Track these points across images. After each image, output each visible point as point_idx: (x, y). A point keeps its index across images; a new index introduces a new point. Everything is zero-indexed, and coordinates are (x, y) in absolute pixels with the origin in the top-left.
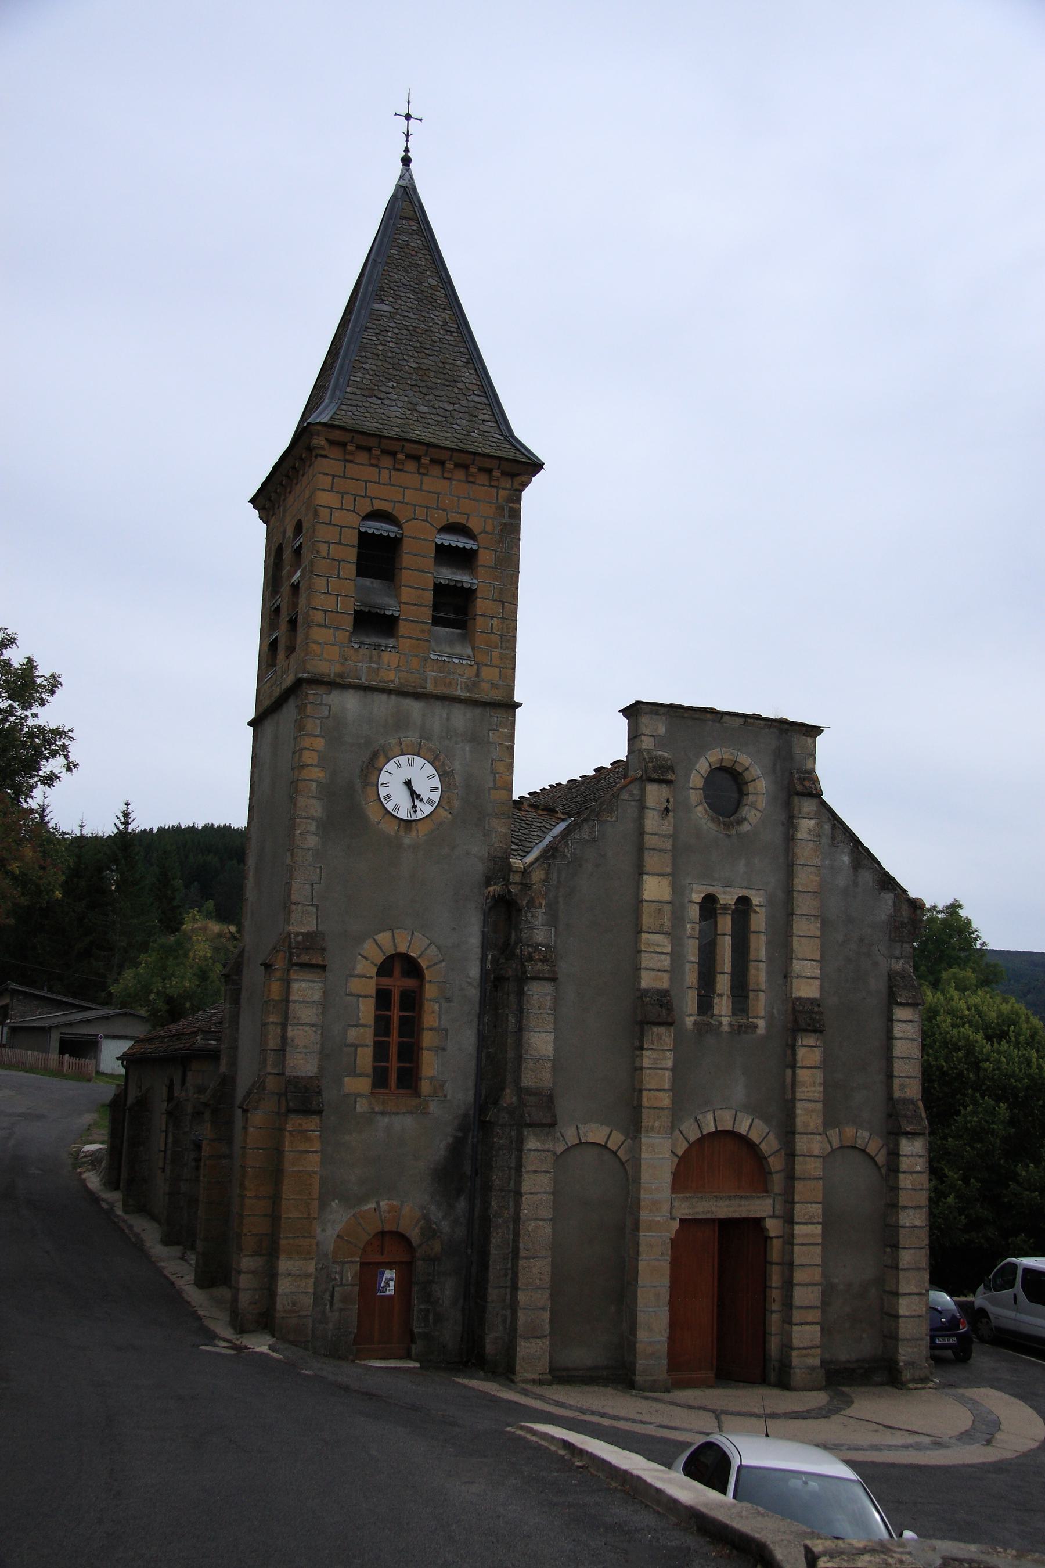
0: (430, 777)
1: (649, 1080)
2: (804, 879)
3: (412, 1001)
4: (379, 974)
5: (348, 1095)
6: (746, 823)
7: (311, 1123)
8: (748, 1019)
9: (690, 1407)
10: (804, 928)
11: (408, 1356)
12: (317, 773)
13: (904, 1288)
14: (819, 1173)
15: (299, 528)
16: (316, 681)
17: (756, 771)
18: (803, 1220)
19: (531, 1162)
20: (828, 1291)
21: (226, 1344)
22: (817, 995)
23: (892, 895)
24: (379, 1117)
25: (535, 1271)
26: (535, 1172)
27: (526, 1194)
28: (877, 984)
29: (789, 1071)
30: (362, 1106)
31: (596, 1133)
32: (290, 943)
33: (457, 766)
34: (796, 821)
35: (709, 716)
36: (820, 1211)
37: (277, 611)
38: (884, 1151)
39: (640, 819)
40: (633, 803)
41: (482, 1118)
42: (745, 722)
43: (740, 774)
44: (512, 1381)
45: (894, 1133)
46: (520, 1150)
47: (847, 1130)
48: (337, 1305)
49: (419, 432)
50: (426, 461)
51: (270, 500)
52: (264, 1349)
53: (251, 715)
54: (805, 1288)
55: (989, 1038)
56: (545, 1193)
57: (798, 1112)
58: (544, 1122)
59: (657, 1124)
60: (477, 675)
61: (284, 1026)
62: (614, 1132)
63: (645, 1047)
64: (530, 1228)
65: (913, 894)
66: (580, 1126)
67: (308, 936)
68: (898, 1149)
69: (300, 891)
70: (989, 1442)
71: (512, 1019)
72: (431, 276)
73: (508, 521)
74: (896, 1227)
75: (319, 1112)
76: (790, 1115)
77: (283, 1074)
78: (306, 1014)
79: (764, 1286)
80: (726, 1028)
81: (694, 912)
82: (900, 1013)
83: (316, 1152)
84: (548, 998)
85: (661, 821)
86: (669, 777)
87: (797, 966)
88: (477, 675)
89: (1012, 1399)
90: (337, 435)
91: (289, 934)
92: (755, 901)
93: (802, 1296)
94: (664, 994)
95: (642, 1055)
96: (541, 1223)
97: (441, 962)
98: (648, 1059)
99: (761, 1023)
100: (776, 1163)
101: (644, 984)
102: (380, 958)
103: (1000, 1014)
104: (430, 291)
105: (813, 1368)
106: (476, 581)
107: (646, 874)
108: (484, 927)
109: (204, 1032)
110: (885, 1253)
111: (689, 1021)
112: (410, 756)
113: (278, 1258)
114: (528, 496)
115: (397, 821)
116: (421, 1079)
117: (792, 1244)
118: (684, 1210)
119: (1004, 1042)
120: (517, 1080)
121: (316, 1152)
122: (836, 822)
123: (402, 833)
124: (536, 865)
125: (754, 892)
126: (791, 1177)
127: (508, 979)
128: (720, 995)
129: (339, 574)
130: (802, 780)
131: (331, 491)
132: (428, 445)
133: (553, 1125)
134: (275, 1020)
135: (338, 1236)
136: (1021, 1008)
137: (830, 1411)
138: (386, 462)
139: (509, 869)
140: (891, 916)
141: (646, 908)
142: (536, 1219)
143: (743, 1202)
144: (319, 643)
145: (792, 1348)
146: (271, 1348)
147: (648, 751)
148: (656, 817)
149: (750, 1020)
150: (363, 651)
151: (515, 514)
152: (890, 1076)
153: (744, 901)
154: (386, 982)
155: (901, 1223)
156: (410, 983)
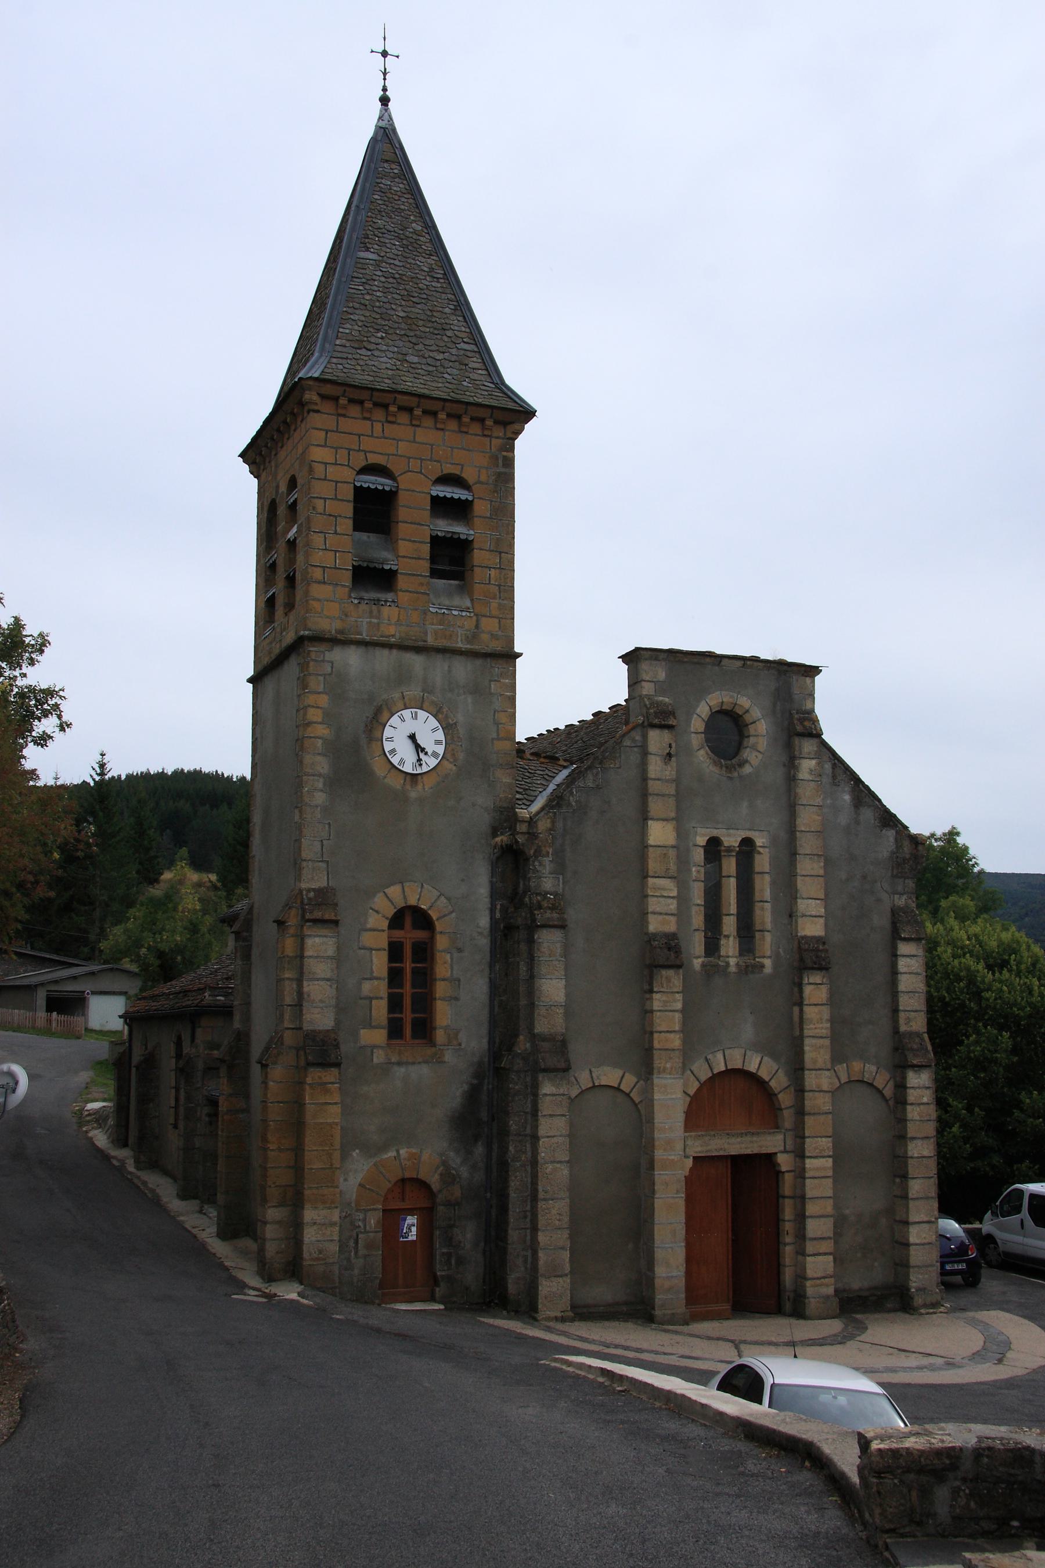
0: (434, 730)
1: (660, 1022)
2: (807, 819)
3: (424, 952)
7: (330, 1075)
8: (754, 960)
9: (709, 1338)
10: (808, 867)
11: (432, 1299)
12: (322, 731)
15: (293, 483)
16: (318, 639)
17: (756, 713)
18: (814, 1154)
19: (546, 1106)
20: (840, 1222)
23: (893, 832)
24: (396, 1068)
25: (554, 1212)
26: (551, 1116)
27: (543, 1137)
28: (881, 920)
29: (796, 1009)
30: (379, 1057)
31: (609, 1076)
32: (302, 898)
33: (460, 718)
35: (708, 660)
37: (273, 567)
38: (891, 1084)
40: (636, 749)
44: (535, 1319)
45: (900, 1067)
46: (535, 1095)
47: (854, 1063)
48: (362, 1251)
49: (409, 383)
51: (260, 454)
52: (294, 1296)
54: (818, 1220)
55: (990, 967)
56: (560, 1136)
57: (807, 1048)
59: (668, 1065)
60: (477, 626)
61: (300, 981)
62: (627, 1074)
66: (593, 1069)
67: (319, 892)
69: (310, 849)
70: (1000, 1361)
72: (415, 221)
73: (503, 470)
74: (906, 1157)
75: (338, 1065)
77: (301, 1028)
78: (320, 969)
79: (777, 1221)
80: (733, 969)
81: (699, 855)
82: (904, 948)
83: (336, 1103)
84: (558, 945)
85: (664, 766)
86: (670, 723)
87: (802, 905)
88: (477, 626)
90: (328, 389)
91: (301, 891)
92: (759, 842)
93: (815, 1227)
94: (673, 936)
96: (558, 1165)
97: (452, 912)
98: (657, 1001)
99: (768, 963)
100: (786, 1100)
101: (652, 928)
102: (391, 912)
103: (1001, 943)
104: (415, 237)
105: (828, 1297)
106: (472, 532)
108: (492, 877)
109: (212, 988)
111: (697, 963)
113: (303, 1208)
114: (521, 444)
116: (435, 1029)
117: (804, 1178)
118: (698, 1148)
119: (1005, 971)
121: (336, 1103)
122: (836, 761)
123: (408, 787)
125: (757, 833)
126: (800, 1112)
128: (727, 937)
129: (336, 531)
130: (801, 721)
133: (567, 1069)
135: (360, 1185)
136: (1022, 937)
137: (844, 1337)
138: (379, 414)
140: (893, 853)
141: (652, 853)
142: (552, 1162)
143: (755, 1139)
144: (319, 600)
145: (806, 1279)
146: (299, 1294)
147: (649, 697)
148: (659, 762)
149: (757, 960)
150: (363, 607)
151: (509, 463)
152: (895, 1011)
153: (747, 842)
154: (398, 934)
155: (910, 1154)
156: (421, 935)
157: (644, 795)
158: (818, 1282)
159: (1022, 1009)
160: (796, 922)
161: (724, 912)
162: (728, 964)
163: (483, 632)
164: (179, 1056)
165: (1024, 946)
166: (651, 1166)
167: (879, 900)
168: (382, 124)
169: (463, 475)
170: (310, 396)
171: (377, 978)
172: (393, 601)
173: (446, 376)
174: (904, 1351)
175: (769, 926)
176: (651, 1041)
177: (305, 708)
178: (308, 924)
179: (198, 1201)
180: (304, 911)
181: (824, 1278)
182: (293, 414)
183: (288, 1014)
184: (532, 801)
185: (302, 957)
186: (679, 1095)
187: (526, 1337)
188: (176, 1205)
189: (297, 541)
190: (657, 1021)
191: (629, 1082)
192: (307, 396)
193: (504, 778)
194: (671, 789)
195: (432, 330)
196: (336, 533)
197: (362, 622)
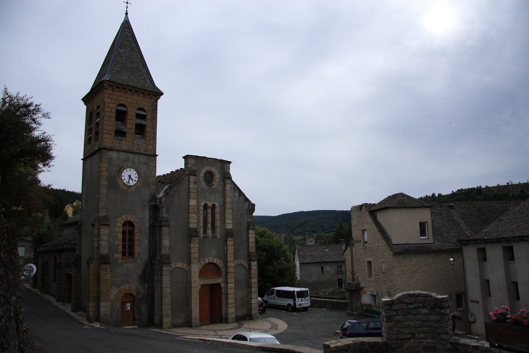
0: (135, 174)
1: (193, 251)
2: (228, 199)
3: (131, 233)
4: (123, 226)
5: (116, 258)
6: (214, 186)
7: (108, 266)
8: (215, 234)
9: (207, 330)
10: (228, 211)
11: (134, 325)
12: (105, 173)
13: (253, 297)
14: (233, 271)
15: (98, 107)
16: (105, 149)
17: (216, 173)
19: (164, 273)
20: (236, 299)
21: (87, 326)
22: (232, 228)
24: (124, 264)
25: (167, 300)
26: (166, 275)
28: (245, 225)
29: (225, 247)
31: (180, 265)
32: (100, 218)
33: (142, 171)
34: (226, 185)
35: (205, 159)
36: (234, 280)
37: (91, 129)
38: (247, 265)
39: (189, 184)
40: (187, 181)
41: (151, 263)
42: (213, 161)
43: (212, 173)
44: (162, 328)
45: (250, 260)
46: (162, 270)
48: (116, 313)
49: (131, 84)
50: (133, 91)
51: (88, 99)
52: (98, 326)
53: (82, 157)
55: (260, 237)
56: (168, 281)
57: (228, 257)
58: (168, 263)
59: (195, 262)
60: (147, 147)
61: (99, 241)
62: (184, 264)
63: (192, 242)
64: (165, 290)
65: (252, 202)
67: (104, 217)
68: (251, 264)
69: (102, 205)
70: (277, 329)
71: (158, 237)
72: (133, 44)
73: (154, 108)
74: (251, 283)
75: (109, 263)
76: (226, 258)
77: (99, 254)
78: (105, 238)
79: (221, 300)
80: (210, 237)
81: (202, 208)
82: (250, 231)
83: (109, 274)
84: (167, 231)
86: (196, 174)
87: (227, 221)
88: (147, 147)
89: (278, 319)
90: (111, 84)
91: (99, 216)
93: (231, 301)
94: (196, 229)
95: (191, 245)
96: (167, 288)
97: (139, 222)
98: (192, 245)
99: (218, 235)
100: (223, 270)
101: (191, 227)
102: (123, 222)
103: (262, 231)
104: (133, 47)
105: (233, 318)
106: (146, 123)
107: (191, 199)
108: (150, 213)
109: (66, 244)
110: (248, 289)
111: (202, 236)
112: (130, 169)
113: (100, 302)
114: (159, 101)
115: (127, 186)
116: (134, 253)
117: (228, 289)
118: (202, 283)
119: (263, 237)
120: (160, 252)
121: (109, 274)
123: (128, 189)
124: (163, 197)
125: (216, 203)
126: (227, 273)
127: (157, 226)
128: (209, 229)
129: (111, 120)
130: (227, 175)
131: (109, 98)
132: (135, 87)
133: (169, 264)
134: (96, 239)
135: (115, 296)
136: (267, 229)
137: (239, 327)
138: (123, 91)
139: (156, 198)
140: (248, 208)
141: (191, 208)
142: (166, 288)
144: (106, 139)
145: (228, 314)
146: (100, 326)
147: (190, 168)
148: (193, 184)
149: (216, 235)
150: (117, 141)
151: (156, 106)
152: (248, 247)
153: (214, 205)
154: (125, 228)
155: (252, 282)
156: (131, 228)
157: (189, 192)
158: (371, 321)
159: (268, 246)
160: (225, 225)
161: (208, 223)
162: (209, 236)
163: (148, 149)
164: (55, 262)
165: (267, 231)
166: (191, 287)
167: (245, 220)
168: (125, 19)
169: (144, 108)
170: (105, 85)
171: (119, 240)
172: (125, 140)
173: (141, 83)
174: (254, 329)
175: (219, 226)
176: (191, 255)
177: (101, 167)
178: (101, 225)
179: (62, 302)
180: (100, 222)
181: (232, 313)
182: (100, 89)
183: (95, 249)
184: (159, 194)
185: (99, 234)
186: (198, 269)
187: (161, 333)
188: (56, 303)
189: (100, 123)
190: (192, 250)
191: (185, 266)
192: (105, 85)
193: (153, 187)
194: (196, 191)
195: (137, 71)
196: (111, 121)
197: (117, 144)
